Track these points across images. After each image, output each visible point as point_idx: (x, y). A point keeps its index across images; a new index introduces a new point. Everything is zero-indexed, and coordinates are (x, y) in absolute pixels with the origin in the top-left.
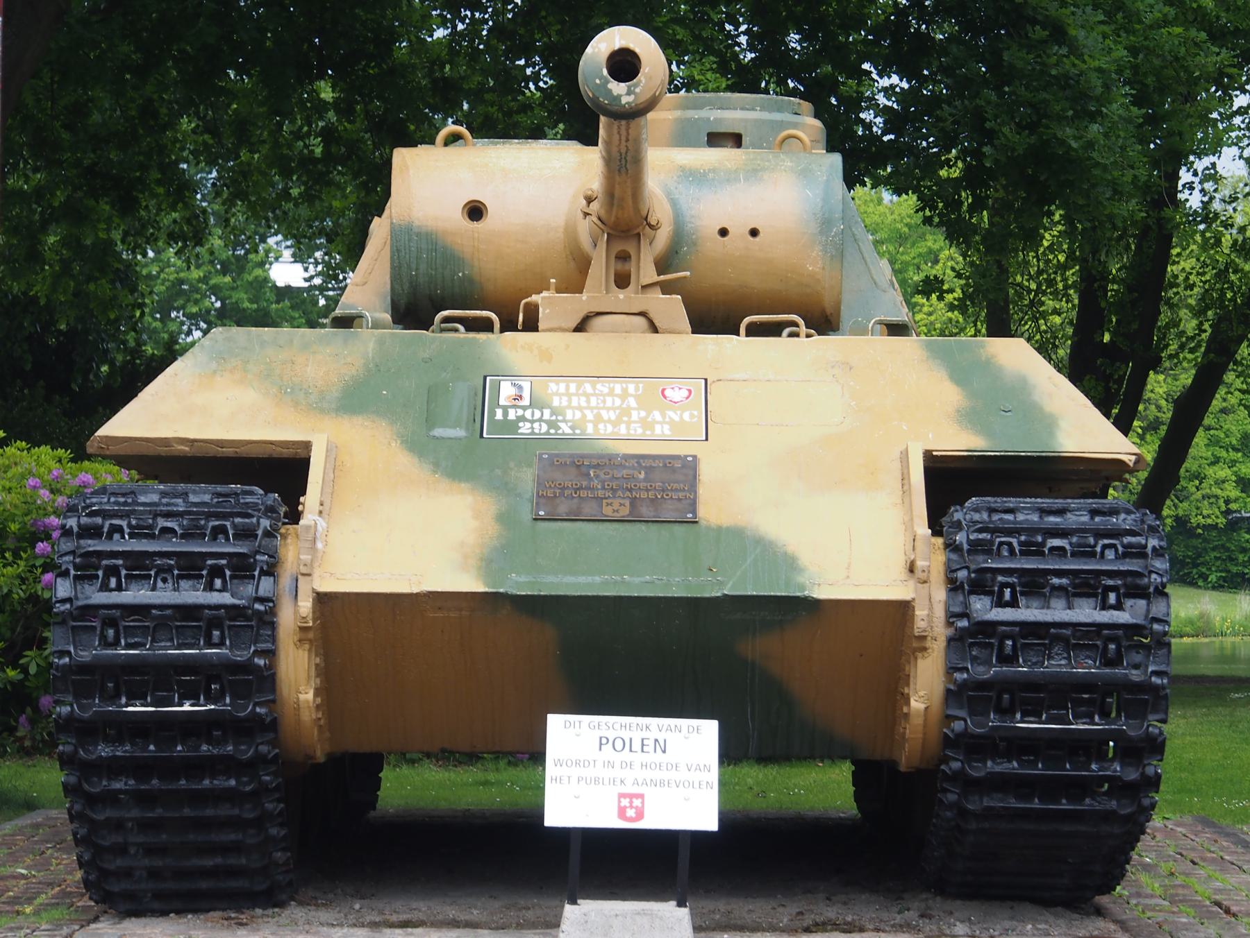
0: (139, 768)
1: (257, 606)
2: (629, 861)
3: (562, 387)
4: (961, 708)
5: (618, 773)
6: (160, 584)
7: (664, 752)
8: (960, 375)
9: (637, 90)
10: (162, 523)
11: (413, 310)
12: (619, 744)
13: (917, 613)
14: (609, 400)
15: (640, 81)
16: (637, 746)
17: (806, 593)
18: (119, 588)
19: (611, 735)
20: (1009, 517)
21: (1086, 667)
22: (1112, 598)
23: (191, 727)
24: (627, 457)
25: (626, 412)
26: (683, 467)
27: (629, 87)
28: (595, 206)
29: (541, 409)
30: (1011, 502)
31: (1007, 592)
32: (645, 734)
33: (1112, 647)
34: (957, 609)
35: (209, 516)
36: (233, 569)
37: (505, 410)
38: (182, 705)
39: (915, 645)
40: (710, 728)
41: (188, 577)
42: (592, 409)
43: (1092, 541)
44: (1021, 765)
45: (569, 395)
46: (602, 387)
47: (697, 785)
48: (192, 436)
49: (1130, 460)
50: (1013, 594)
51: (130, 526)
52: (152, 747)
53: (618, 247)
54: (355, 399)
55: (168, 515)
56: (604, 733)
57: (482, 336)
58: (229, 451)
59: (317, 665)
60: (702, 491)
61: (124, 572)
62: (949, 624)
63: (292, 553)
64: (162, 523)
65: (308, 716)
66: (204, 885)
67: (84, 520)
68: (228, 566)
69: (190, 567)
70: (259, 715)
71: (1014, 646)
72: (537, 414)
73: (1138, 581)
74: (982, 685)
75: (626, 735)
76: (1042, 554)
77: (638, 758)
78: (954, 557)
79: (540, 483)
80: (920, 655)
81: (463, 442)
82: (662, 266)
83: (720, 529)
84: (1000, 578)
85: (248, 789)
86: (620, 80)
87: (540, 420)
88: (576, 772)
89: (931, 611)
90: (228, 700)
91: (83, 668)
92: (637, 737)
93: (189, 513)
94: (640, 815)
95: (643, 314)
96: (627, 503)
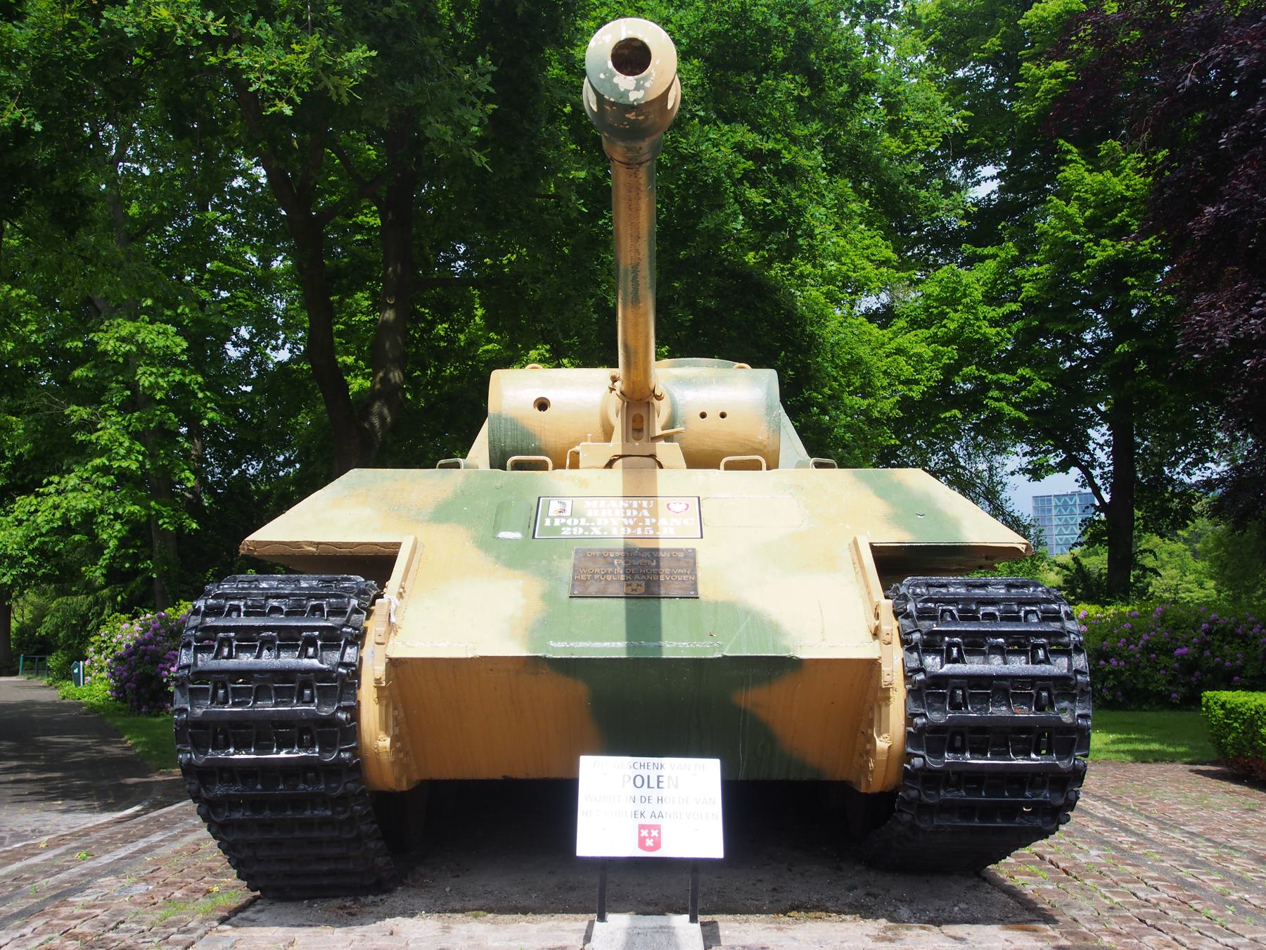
0: (256, 804)
2: (649, 883)
6: (265, 652)
8: (883, 492)
9: (647, 84)
10: (275, 603)
11: (498, 461)
16: (653, 783)
17: (791, 654)
18: (230, 656)
20: (944, 590)
21: (1024, 712)
22: (1041, 653)
24: (643, 550)
25: (642, 519)
28: (618, 384)
29: (579, 518)
30: (944, 580)
31: (955, 650)
32: (659, 772)
33: (1044, 694)
34: (914, 665)
35: (309, 597)
36: (324, 639)
38: (278, 753)
43: (1016, 608)
44: (968, 794)
49: (1022, 548)
50: (959, 651)
51: (245, 605)
52: (259, 787)
53: (635, 412)
54: (443, 514)
55: (277, 597)
59: (395, 718)
60: (699, 574)
61: (235, 643)
62: (906, 678)
63: (374, 627)
64: (275, 603)
65: (386, 758)
66: (325, 882)
67: (211, 601)
68: (319, 637)
69: (289, 639)
71: (964, 695)
74: (936, 729)
75: (645, 773)
76: (977, 619)
78: (906, 622)
79: (576, 569)
83: (716, 603)
85: (341, 817)
87: (578, 526)
89: (893, 664)
91: (198, 724)
92: (654, 775)
93: (294, 595)
94: (657, 845)
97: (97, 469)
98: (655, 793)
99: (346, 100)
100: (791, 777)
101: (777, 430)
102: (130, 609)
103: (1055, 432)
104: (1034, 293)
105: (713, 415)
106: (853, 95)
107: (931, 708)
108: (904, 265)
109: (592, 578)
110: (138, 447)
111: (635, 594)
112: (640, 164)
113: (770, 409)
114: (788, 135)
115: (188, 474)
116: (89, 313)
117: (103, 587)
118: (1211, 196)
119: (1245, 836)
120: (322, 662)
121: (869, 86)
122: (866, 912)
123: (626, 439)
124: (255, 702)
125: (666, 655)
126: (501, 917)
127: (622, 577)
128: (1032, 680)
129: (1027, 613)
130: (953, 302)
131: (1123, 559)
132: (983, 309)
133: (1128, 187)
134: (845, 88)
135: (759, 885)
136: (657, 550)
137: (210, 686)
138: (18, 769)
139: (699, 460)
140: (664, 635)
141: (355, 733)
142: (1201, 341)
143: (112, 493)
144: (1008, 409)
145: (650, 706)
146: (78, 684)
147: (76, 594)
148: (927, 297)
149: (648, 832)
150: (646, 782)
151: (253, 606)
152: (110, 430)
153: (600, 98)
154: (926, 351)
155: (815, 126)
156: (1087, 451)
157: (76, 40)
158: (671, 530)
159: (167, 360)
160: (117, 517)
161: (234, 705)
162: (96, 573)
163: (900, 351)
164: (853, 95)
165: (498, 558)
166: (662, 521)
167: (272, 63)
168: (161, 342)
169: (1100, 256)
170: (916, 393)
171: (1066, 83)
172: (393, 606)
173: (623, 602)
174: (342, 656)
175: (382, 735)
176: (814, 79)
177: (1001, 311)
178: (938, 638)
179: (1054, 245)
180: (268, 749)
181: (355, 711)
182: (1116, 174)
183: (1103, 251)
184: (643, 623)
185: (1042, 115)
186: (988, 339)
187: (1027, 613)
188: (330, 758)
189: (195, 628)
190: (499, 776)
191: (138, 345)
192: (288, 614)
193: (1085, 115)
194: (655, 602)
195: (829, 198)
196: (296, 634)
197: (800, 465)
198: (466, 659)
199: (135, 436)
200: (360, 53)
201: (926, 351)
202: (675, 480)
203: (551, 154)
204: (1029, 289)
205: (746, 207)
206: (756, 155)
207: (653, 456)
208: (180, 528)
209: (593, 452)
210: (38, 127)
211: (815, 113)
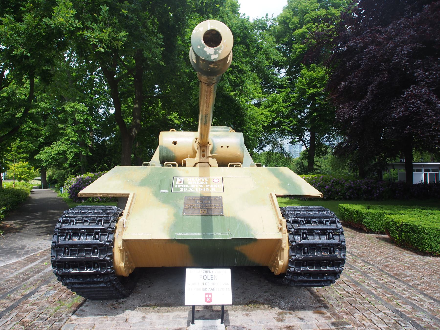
1: (107, 243)
8: (278, 175)
9: (220, 52)
11: (162, 162)
15: (221, 47)
16: (210, 278)
18: (69, 239)
21: (326, 255)
24: (206, 197)
25: (205, 185)
26: (219, 199)
27: (215, 50)
28: (198, 140)
32: (211, 274)
37: (178, 185)
38: (86, 270)
40: (228, 271)
43: (322, 220)
48: (103, 193)
50: (306, 235)
53: (203, 149)
54: (143, 183)
55: (87, 217)
57: (174, 167)
60: (224, 206)
63: (119, 225)
67: (64, 218)
68: (100, 232)
70: (109, 272)
79: (185, 204)
81: (167, 193)
82: (212, 152)
83: (229, 217)
86: (211, 46)
89: (285, 238)
92: (210, 274)
94: (211, 301)
95: (208, 163)
96: (206, 210)
97: (65, 140)
98: (210, 281)
99: (120, 48)
101: (243, 151)
102: (75, 174)
103: (297, 133)
104: (294, 101)
105: (225, 147)
106: (257, 51)
107: (297, 253)
108: (263, 93)
109: (190, 208)
110: (76, 134)
111: (204, 214)
112: (213, 84)
113: (241, 145)
114: (241, 61)
115: (89, 141)
116: (62, 100)
117: (68, 168)
118: (343, 79)
119: (355, 248)
120: (101, 241)
121: (261, 49)
122: (272, 304)
123: (200, 158)
124: (78, 254)
125: (215, 238)
126: (162, 308)
127: (200, 207)
128: (328, 245)
129: (326, 221)
130: (275, 102)
131: (311, 163)
132: (282, 104)
133: (317, 76)
134: (255, 49)
136: (210, 197)
138: (40, 223)
139: (223, 163)
140: (214, 230)
142: (341, 117)
143: (70, 146)
144: (287, 128)
145: (209, 253)
146: (61, 193)
147: (62, 169)
148: (269, 100)
149: (208, 296)
150: (207, 278)
151: (78, 220)
152: (69, 130)
153: (197, 57)
154: (268, 114)
155: (248, 59)
156: (304, 137)
157: (39, 29)
158: (214, 190)
159: (83, 113)
160: (71, 152)
162: (67, 165)
163: (262, 114)
164: (257, 51)
165: (160, 200)
166: (212, 186)
167: (97, 36)
168: (81, 108)
169: (310, 92)
170: (266, 124)
171: (304, 50)
172: (125, 222)
173: (200, 217)
174: (108, 238)
175: (121, 263)
176: (248, 47)
177: (286, 104)
178: (299, 231)
179: (299, 89)
180: (83, 269)
181: (112, 257)
182: (314, 72)
183: (310, 91)
184: (207, 226)
185: (298, 58)
186: (283, 111)
187: (326, 221)
188: (104, 271)
189: (58, 228)
190: (161, 266)
191: (75, 109)
193: (310, 57)
194: (210, 217)
195: (251, 78)
196: (92, 231)
197: (252, 166)
199: (76, 132)
200: (123, 34)
201: (268, 114)
202: (216, 171)
203: (179, 65)
204: (293, 100)
205: (230, 81)
207: (208, 163)
208: (87, 155)
210: (29, 54)
211: (248, 55)
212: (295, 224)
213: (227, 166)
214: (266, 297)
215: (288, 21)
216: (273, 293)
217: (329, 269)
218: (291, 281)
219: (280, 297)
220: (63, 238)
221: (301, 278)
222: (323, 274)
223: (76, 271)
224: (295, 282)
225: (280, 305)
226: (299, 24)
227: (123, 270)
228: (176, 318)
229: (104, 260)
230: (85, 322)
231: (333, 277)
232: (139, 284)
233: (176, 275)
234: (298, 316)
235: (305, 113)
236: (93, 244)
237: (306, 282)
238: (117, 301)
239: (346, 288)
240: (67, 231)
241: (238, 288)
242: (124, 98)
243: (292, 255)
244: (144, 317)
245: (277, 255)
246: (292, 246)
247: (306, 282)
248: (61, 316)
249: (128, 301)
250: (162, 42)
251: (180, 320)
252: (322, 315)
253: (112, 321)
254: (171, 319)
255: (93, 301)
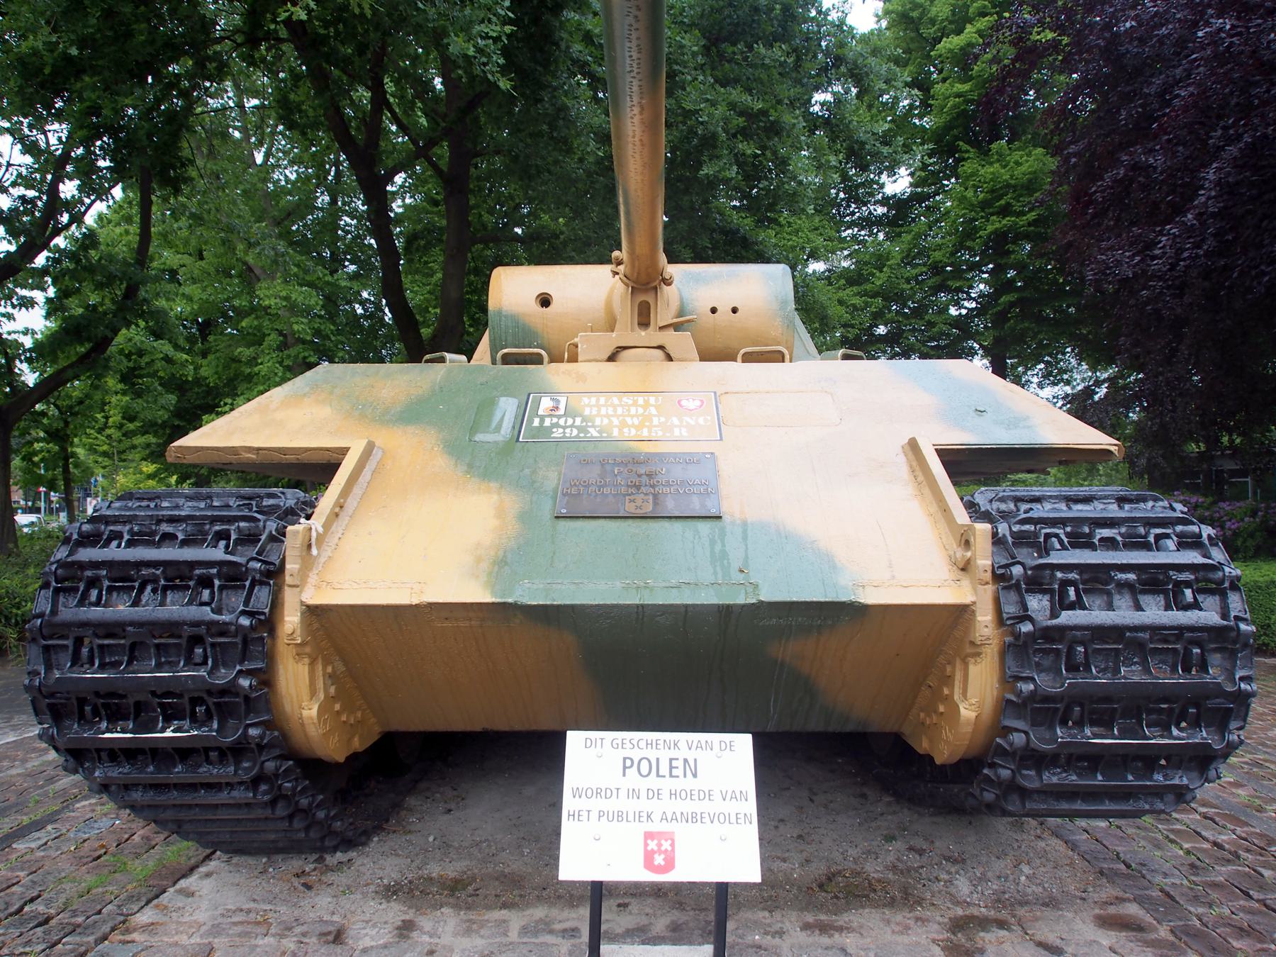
3: (593, 400)
4: (1025, 719)
5: (644, 805)
7: (695, 775)
10: (165, 528)
12: (645, 767)
13: (979, 618)
14: (633, 411)
16: (664, 770)
17: (853, 598)
19: (636, 755)
21: (1165, 677)
22: (1188, 593)
23: (183, 752)
31: (1072, 591)
32: (673, 753)
37: (542, 419)
38: (163, 731)
39: (969, 650)
40: (743, 744)
41: (175, 588)
42: (618, 417)
43: (1142, 530)
45: (598, 406)
46: (627, 400)
47: (733, 819)
50: (1077, 591)
51: (131, 532)
54: (412, 414)
56: (628, 753)
58: (291, 458)
64: (165, 528)
69: (178, 577)
72: (570, 421)
73: (1211, 575)
75: (652, 754)
77: (667, 784)
80: (972, 660)
84: (1059, 575)
87: (572, 426)
88: (597, 804)
90: (215, 726)
92: (664, 756)
94: (669, 865)
95: (661, 347)
100: (830, 729)
107: (1039, 668)
124: (130, 663)
133: (1012, 177)
135: (782, 827)
137: (69, 642)
141: (268, 702)
151: (140, 533)
154: (857, 301)
161: (103, 667)
169: (990, 228)
181: (266, 679)
183: (995, 224)
190: (478, 728)
192: (184, 543)
196: (186, 571)
198: (411, 606)
206: (745, 113)
209: (593, 344)
212: (1025, 551)
213: (735, 360)
214: (891, 858)
215: (915, 14)
216: (919, 843)
217: (1179, 736)
218: (1012, 788)
219: (948, 859)
220: (73, 601)
221: (1052, 778)
222: (1148, 760)
223: (123, 731)
224: (1024, 793)
225: (953, 891)
226: (951, 22)
227: (314, 732)
228: (536, 933)
229: (230, 690)
230: (176, 938)
231: (1195, 774)
232: (411, 801)
233: (531, 756)
234: (1038, 938)
235: (974, 299)
236: (184, 623)
237: (1072, 794)
238: (321, 860)
239: (1206, 828)
240: (89, 573)
241: (782, 820)
242: (417, 250)
243: (1018, 678)
244: (406, 928)
245: (948, 680)
246: (1017, 636)
247: (1072, 794)
248: (99, 912)
249: (359, 862)
250: (508, 9)
251: (549, 939)
252: (1139, 935)
253: (282, 936)
254: (513, 935)
255: (235, 860)
